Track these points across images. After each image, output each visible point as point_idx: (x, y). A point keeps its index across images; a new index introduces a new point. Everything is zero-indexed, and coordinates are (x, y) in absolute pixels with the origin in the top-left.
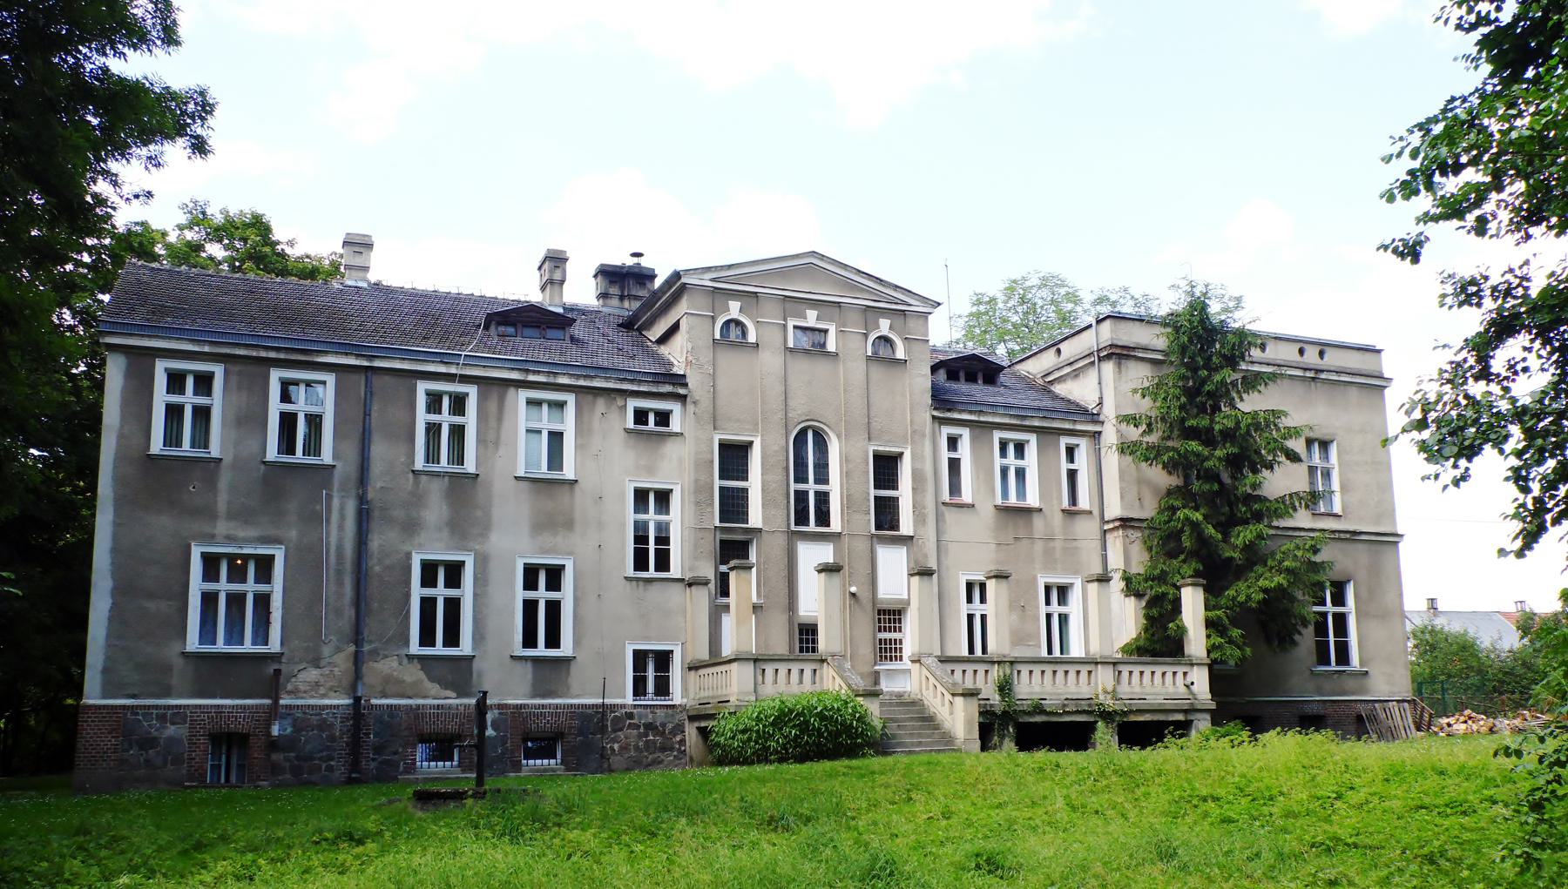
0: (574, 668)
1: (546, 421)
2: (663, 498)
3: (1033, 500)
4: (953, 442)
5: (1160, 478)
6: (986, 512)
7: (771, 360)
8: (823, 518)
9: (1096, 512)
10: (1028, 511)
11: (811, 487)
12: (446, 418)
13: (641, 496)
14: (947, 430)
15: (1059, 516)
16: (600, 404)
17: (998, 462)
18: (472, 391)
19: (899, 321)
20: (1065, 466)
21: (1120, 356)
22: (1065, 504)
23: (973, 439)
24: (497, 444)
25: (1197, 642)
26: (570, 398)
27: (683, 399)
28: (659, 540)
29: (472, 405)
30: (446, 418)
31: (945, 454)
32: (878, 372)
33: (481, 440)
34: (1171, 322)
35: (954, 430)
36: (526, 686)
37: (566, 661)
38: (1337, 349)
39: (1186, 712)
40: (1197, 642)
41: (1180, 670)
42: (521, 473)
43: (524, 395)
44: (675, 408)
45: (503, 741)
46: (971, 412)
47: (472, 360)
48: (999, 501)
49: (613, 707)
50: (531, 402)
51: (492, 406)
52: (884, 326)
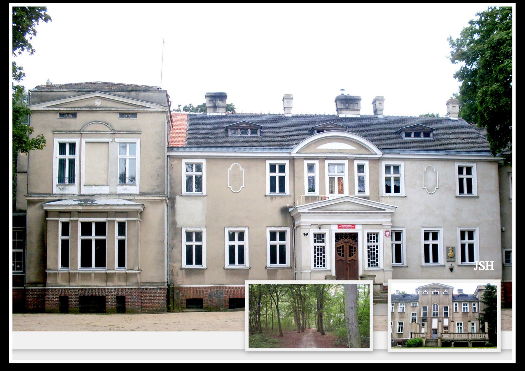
0: (403, 334)
1: (402, 306)
2: (416, 314)
3: (468, 311)
4: (456, 305)
5: (486, 306)
6: (460, 313)
7: (430, 296)
8: (437, 315)
9: (478, 312)
10: (468, 313)
11: (435, 312)
12: (465, 306)
13: (413, 314)
14: (455, 303)
15: (472, 313)
16: (408, 304)
17: (463, 306)
18: (468, 303)
19: (448, 290)
20: (473, 306)
21: (480, 291)
22: (473, 311)
23: (459, 304)
24: (396, 309)
25: (486, 330)
26: (405, 303)
27: (418, 302)
28: (415, 319)
29: (468, 305)
30: (465, 306)
31: (454, 306)
32: (444, 296)
33: (395, 309)
34: (486, 286)
35: (456, 303)
36: (397, 337)
37: (403, 333)
38: (100, 144)
39: (484, 341)
40: (486, 330)
41: (484, 334)
42: (399, 312)
43: (400, 303)
44: (417, 303)
45: (395, 343)
46: (154, 286)
47: (395, 300)
48: (463, 312)
49: (408, 339)
50: (401, 304)
51: (396, 305)
52: (446, 291)
